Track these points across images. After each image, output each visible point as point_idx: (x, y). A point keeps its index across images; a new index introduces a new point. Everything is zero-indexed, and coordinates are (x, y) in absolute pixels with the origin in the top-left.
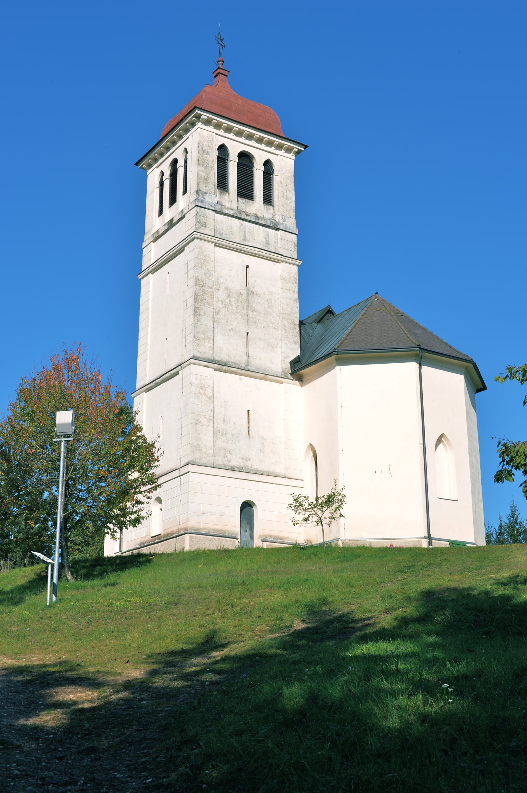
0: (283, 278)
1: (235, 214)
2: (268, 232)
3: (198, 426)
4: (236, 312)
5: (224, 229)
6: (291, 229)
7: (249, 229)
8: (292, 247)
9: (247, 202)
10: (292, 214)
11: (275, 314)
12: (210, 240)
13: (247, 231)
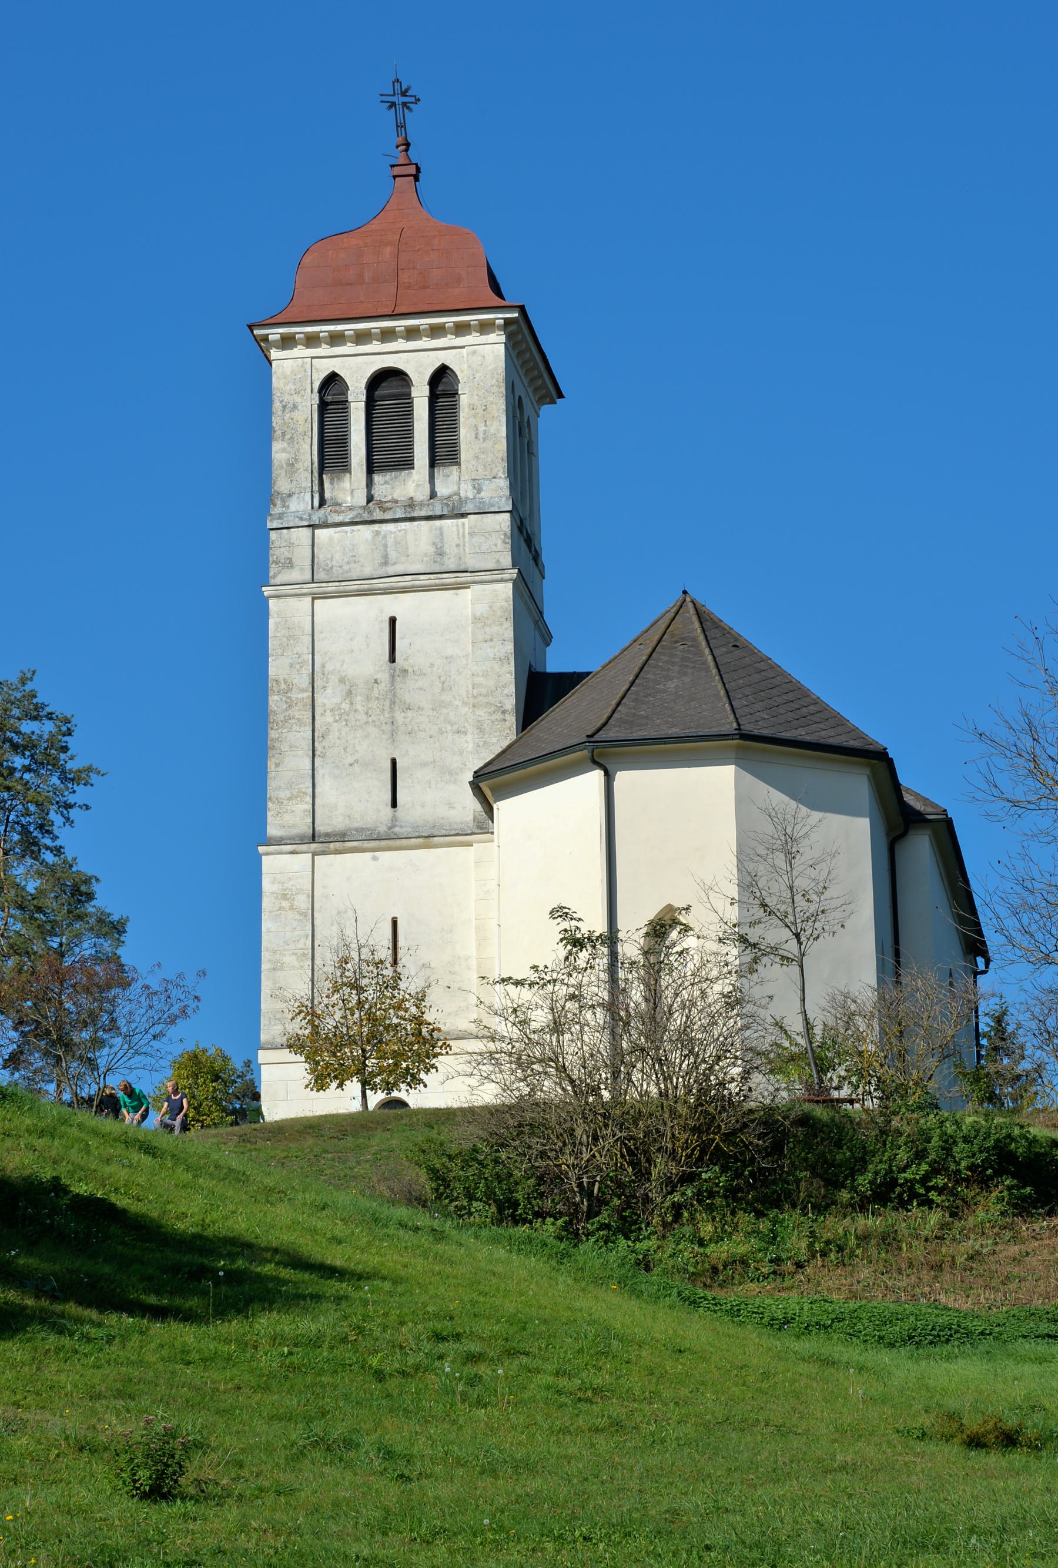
0: (476, 619)
1: (356, 516)
2: (441, 529)
3: (278, 973)
4: (367, 723)
5: (338, 557)
6: (492, 506)
7: (395, 538)
8: (499, 542)
9: (396, 477)
10: (501, 469)
11: (457, 703)
12: (298, 591)
13: (390, 542)
